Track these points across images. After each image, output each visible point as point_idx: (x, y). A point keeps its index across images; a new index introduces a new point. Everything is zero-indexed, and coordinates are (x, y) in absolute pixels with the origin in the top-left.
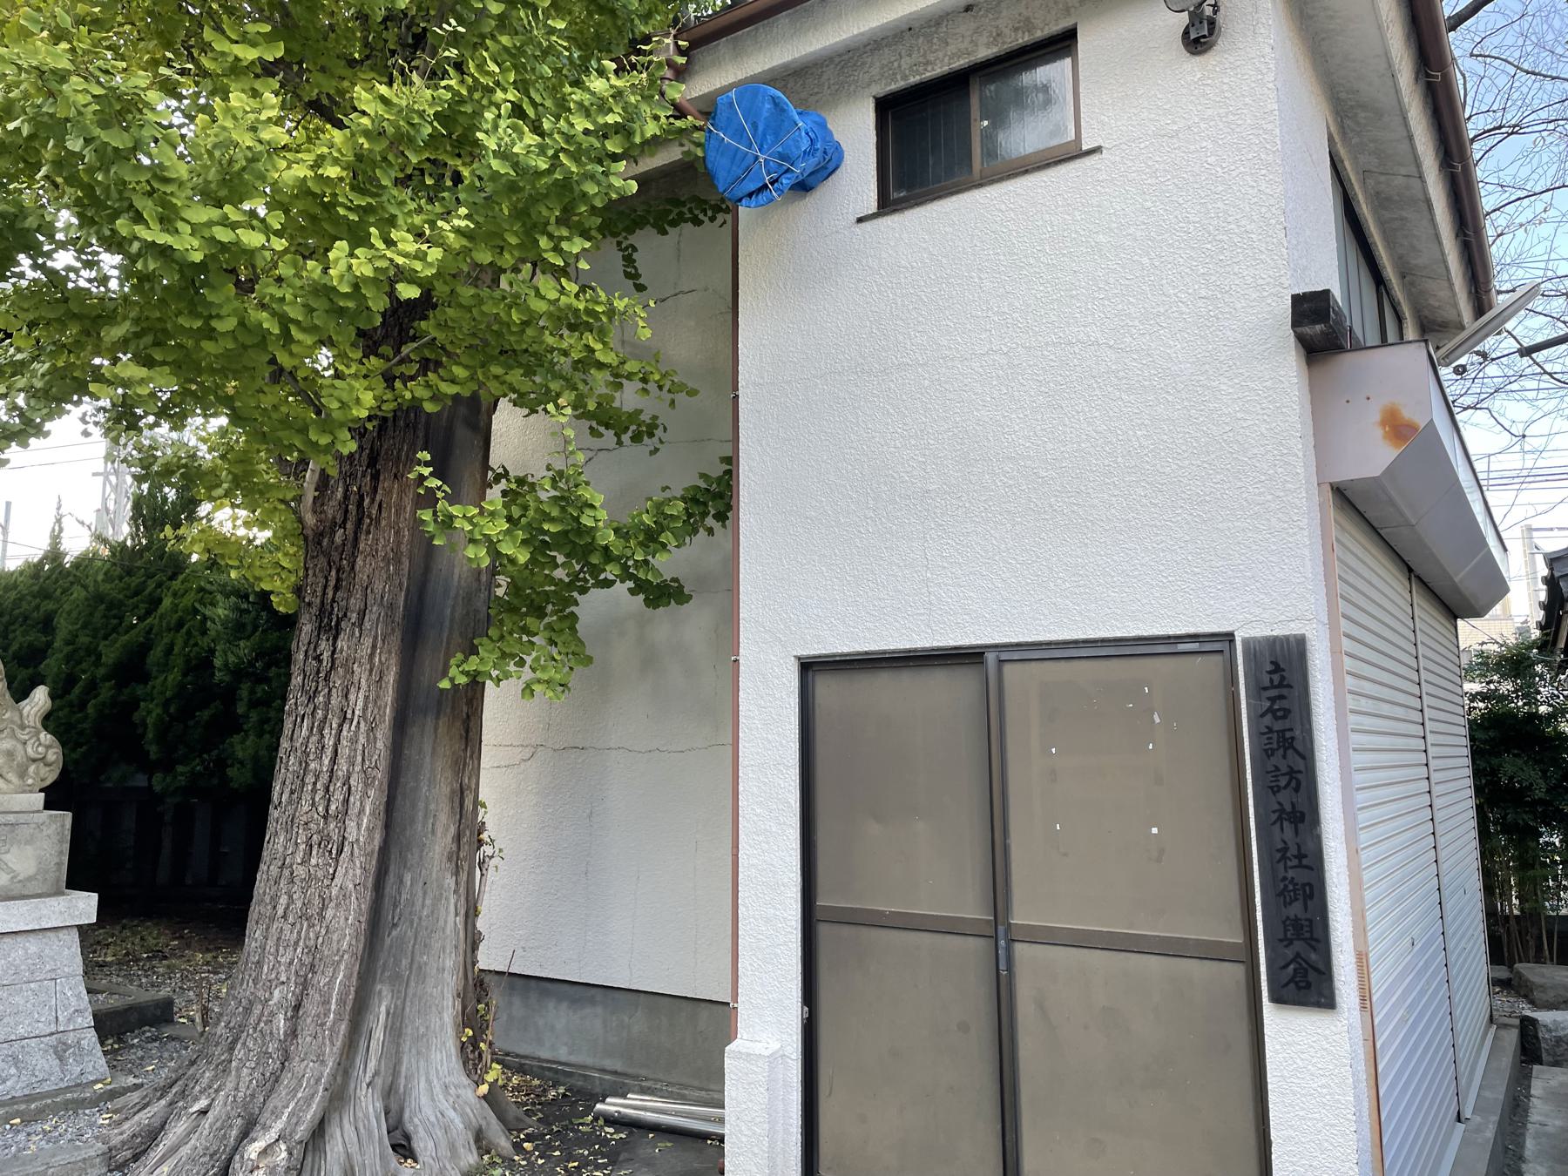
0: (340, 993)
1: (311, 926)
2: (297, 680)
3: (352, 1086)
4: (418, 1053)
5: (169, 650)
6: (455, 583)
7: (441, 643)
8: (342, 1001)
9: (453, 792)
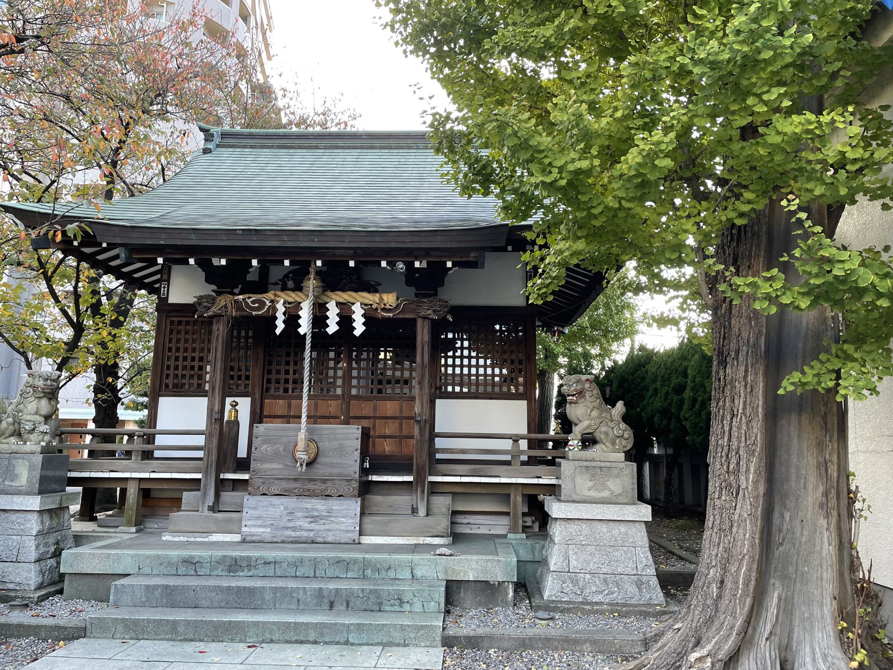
1: (726, 536)
3: (757, 637)
6: (804, 324)
8: (746, 584)
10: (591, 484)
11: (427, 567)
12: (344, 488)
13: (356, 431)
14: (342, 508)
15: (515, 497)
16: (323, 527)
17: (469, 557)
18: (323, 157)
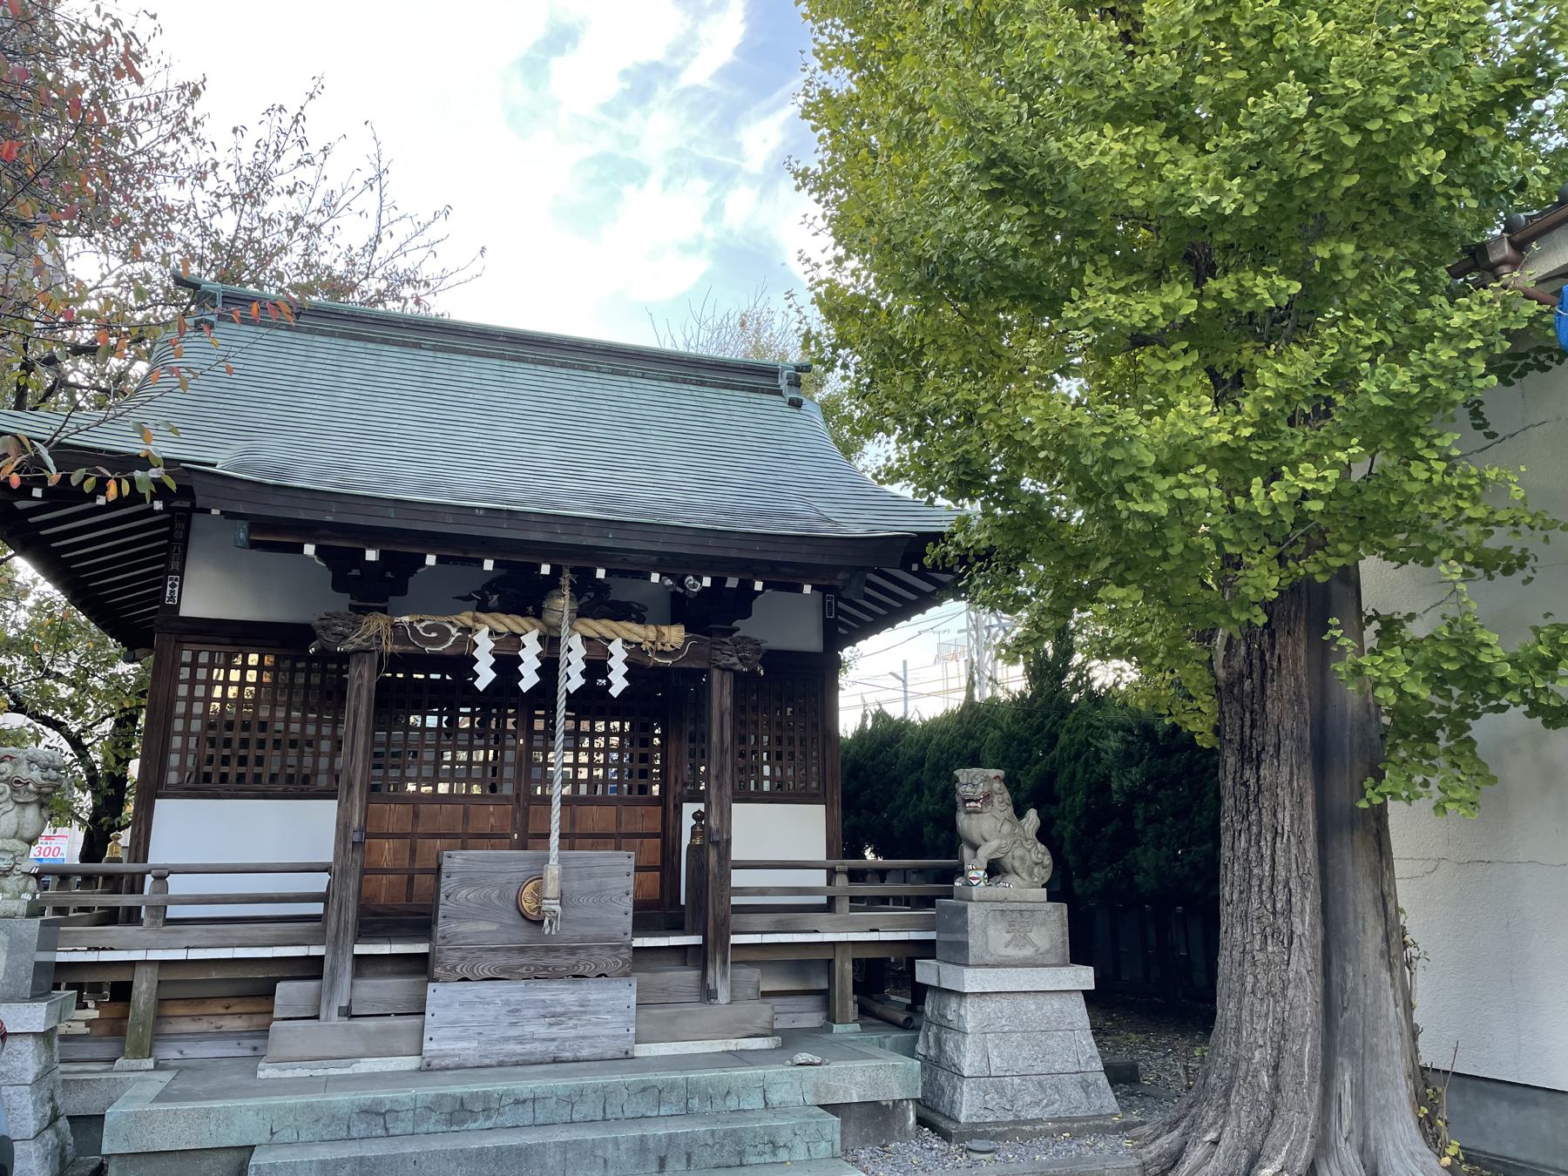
0: (1311, 1060)
2: (1228, 802)
4: (1383, 1120)
5: (1073, 776)
7: (1350, 770)
8: (1312, 1067)
9: (1375, 898)
10: (1008, 937)
11: (787, 1087)
12: (606, 960)
13: (626, 861)
14: (605, 996)
15: (842, 964)
16: (572, 1033)
17: (851, 1064)
18: (362, 356)
